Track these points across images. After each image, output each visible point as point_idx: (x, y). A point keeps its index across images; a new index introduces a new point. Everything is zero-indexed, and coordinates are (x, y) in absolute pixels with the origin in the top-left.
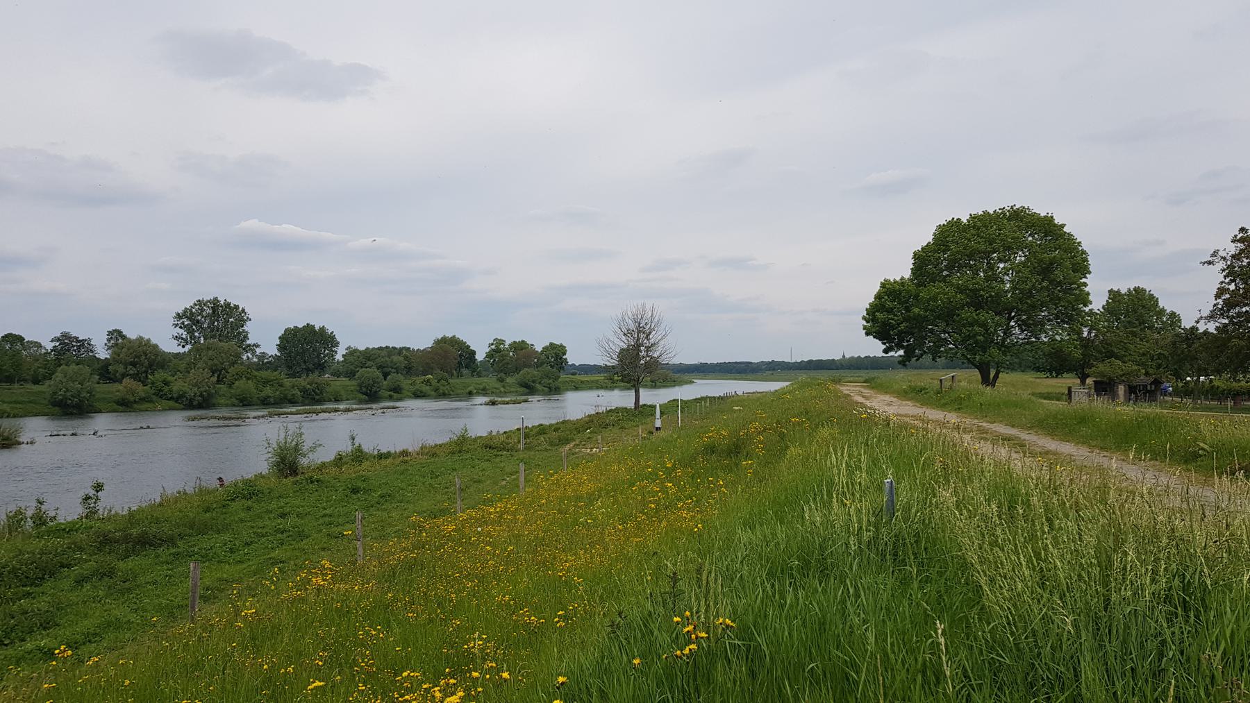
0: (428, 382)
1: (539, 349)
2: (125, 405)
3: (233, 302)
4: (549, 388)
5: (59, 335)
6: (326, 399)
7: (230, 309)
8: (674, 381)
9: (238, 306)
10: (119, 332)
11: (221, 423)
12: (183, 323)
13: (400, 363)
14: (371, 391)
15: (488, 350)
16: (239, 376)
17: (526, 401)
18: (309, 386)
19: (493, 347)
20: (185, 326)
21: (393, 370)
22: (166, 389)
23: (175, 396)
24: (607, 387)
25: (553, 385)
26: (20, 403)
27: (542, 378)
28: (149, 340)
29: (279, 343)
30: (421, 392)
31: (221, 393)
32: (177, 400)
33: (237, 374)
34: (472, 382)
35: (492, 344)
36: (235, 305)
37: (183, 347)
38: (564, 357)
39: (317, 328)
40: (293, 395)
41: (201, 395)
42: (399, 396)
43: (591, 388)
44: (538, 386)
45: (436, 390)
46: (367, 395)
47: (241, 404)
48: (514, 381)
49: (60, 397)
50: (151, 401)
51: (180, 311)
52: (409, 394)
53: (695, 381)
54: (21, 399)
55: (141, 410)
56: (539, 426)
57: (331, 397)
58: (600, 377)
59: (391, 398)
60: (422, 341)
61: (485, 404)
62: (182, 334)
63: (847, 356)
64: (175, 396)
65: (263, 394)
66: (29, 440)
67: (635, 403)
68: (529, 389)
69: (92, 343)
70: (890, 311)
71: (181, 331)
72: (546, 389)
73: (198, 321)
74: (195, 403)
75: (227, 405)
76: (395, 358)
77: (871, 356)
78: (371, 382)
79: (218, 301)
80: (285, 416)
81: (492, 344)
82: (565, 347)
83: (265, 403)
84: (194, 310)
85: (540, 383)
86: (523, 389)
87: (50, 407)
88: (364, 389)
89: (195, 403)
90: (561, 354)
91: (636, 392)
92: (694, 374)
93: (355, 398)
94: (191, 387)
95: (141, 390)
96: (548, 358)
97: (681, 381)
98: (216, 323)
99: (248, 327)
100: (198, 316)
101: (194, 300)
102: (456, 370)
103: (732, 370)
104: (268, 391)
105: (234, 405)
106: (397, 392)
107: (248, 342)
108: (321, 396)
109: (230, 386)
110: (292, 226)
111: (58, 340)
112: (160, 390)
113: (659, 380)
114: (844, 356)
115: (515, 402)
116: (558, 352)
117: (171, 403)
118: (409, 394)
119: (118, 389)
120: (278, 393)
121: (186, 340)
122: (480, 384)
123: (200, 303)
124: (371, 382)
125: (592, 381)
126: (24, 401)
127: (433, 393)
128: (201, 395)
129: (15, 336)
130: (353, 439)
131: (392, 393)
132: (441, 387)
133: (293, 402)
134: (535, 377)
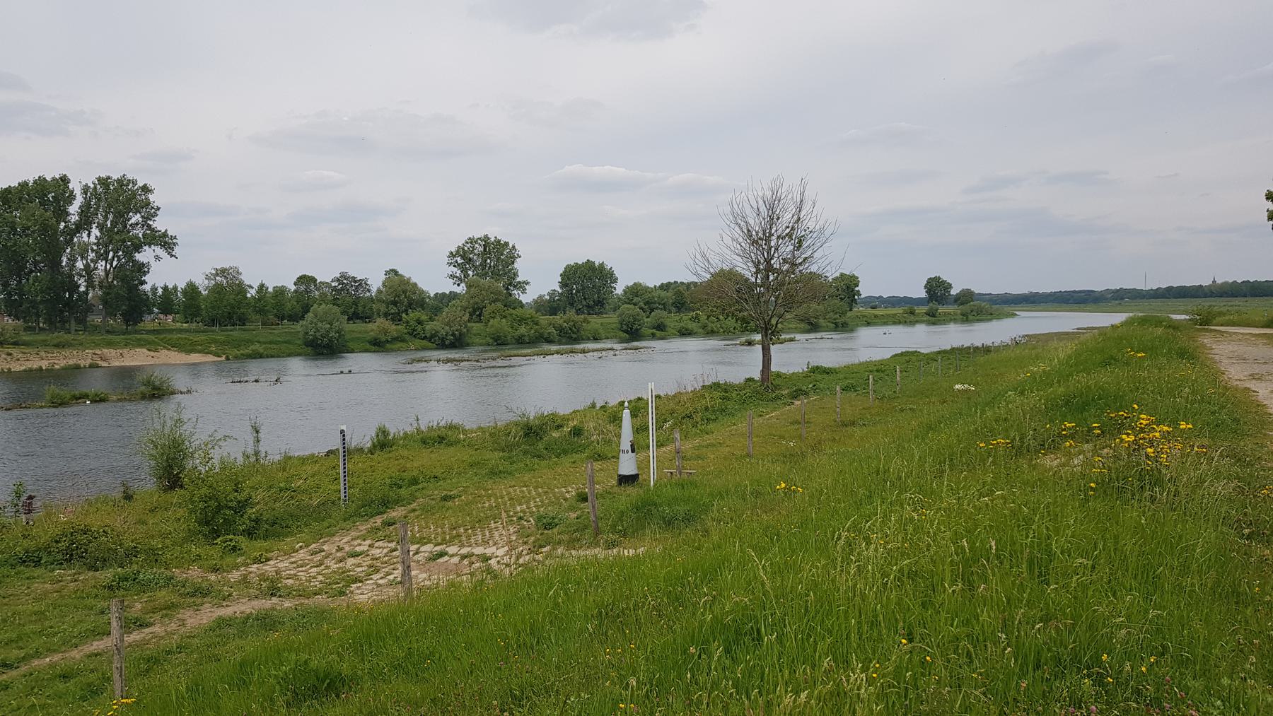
0: (696, 319)
2: (378, 345)
4: (835, 324)
5: (338, 275)
6: (584, 337)
8: (992, 314)
9: (508, 243)
12: (457, 262)
14: (631, 329)
18: (565, 324)
21: (661, 307)
22: (419, 328)
23: (428, 335)
24: (905, 322)
26: (275, 344)
28: (409, 279)
29: (560, 280)
30: (686, 330)
32: (430, 339)
37: (458, 285)
38: (857, 289)
41: (453, 335)
45: (704, 327)
47: (496, 343)
50: (403, 341)
51: (453, 250)
53: (1017, 313)
55: (393, 350)
57: (589, 335)
58: (898, 311)
59: (653, 337)
63: (1219, 281)
64: (428, 335)
66: (185, 390)
67: (763, 371)
69: (368, 283)
71: (455, 270)
73: (470, 260)
74: (447, 342)
75: (481, 345)
78: (631, 319)
79: (489, 239)
80: (508, 358)
83: (521, 342)
84: (466, 248)
87: (304, 346)
88: (625, 327)
89: (447, 342)
91: (763, 349)
92: (1022, 305)
93: (616, 337)
95: (394, 329)
97: (1000, 314)
98: (489, 261)
99: (518, 265)
100: (470, 254)
103: (1069, 300)
104: (523, 330)
105: (489, 345)
106: (660, 331)
107: (518, 279)
110: (608, 167)
111: (338, 280)
112: (414, 330)
113: (972, 314)
114: (1214, 281)
117: (425, 342)
120: (532, 331)
121: (460, 279)
123: (472, 241)
124: (631, 319)
125: (889, 316)
126: (279, 341)
127: (701, 330)
128: (453, 335)
129: (309, 277)
131: (654, 331)
132: (710, 324)
133: (550, 341)
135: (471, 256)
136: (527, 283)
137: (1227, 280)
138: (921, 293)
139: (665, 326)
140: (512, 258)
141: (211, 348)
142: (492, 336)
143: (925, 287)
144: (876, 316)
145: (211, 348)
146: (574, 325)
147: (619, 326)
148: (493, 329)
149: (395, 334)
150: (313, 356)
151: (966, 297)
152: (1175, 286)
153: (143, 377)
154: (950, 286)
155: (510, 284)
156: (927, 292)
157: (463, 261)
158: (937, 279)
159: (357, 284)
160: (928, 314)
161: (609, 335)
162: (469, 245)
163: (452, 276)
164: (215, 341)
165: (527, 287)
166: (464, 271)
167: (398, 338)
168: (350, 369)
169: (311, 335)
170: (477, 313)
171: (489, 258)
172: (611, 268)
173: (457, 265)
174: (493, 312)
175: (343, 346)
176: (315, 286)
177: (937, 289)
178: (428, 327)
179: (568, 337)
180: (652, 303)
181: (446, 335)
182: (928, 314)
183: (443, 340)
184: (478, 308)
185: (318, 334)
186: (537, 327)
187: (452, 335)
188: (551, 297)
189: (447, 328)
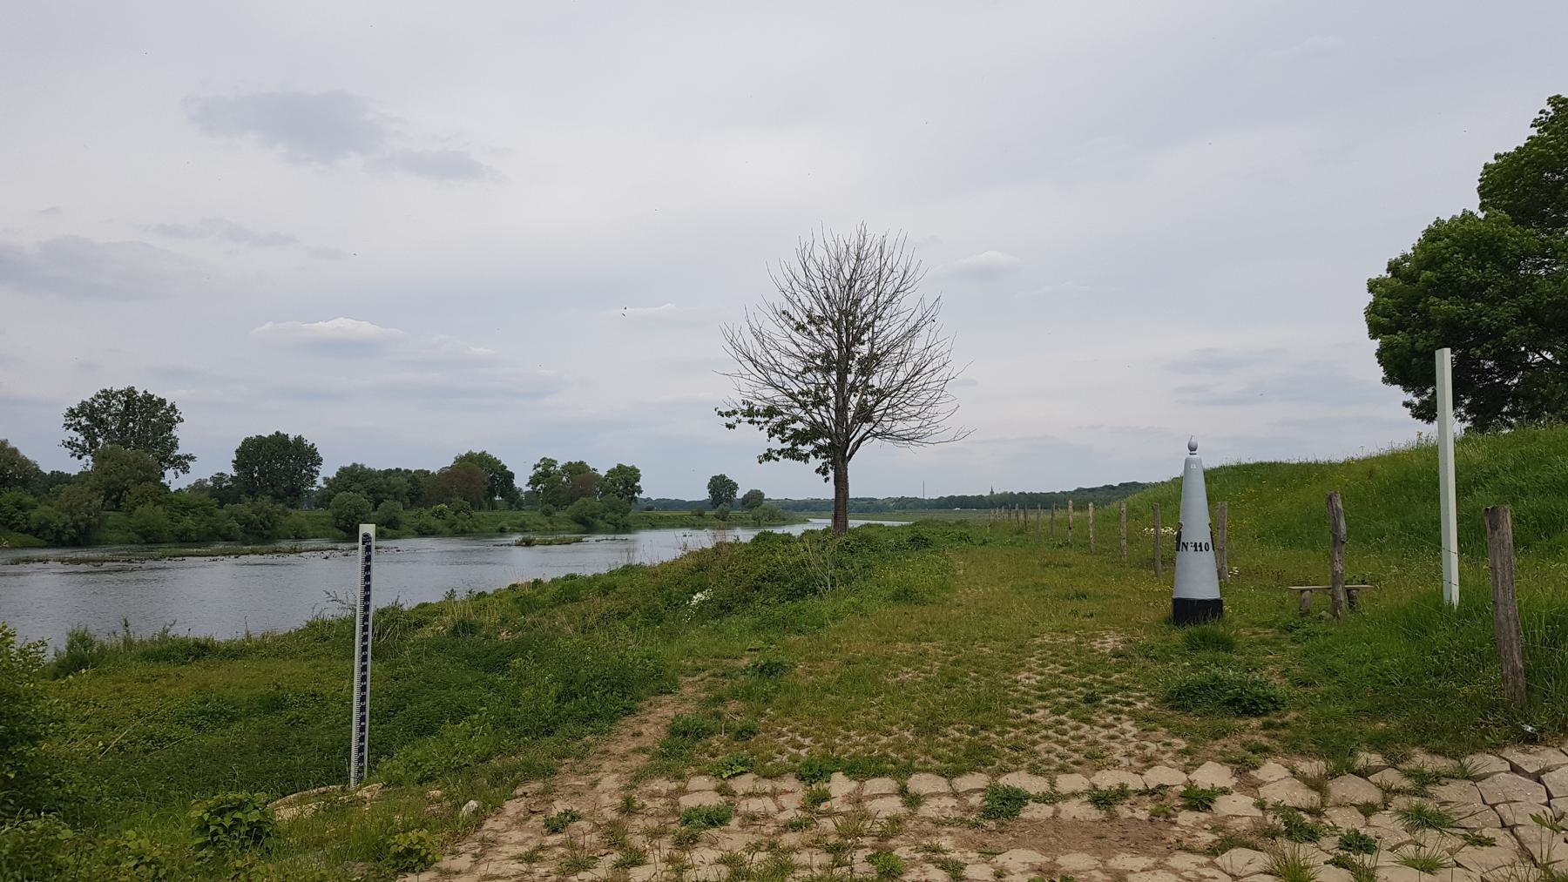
1: (603, 473)
3: (158, 394)
7: (151, 404)
9: (165, 400)
11: (90, 567)
12: (79, 423)
13: (401, 485)
15: (532, 474)
16: (142, 500)
17: (579, 541)
19: (540, 469)
20: (82, 428)
22: (19, 515)
23: (34, 526)
24: (694, 525)
25: (620, 521)
27: (605, 511)
29: (235, 459)
30: (428, 528)
31: (109, 523)
33: (142, 496)
34: (506, 516)
35: (539, 466)
36: (160, 399)
37: (80, 457)
38: (637, 484)
39: (291, 438)
40: (229, 528)
41: (76, 526)
42: (395, 532)
43: (673, 526)
44: (599, 522)
45: (451, 525)
46: (345, 531)
48: (566, 515)
52: (411, 530)
53: (811, 520)
56: (566, 578)
57: (289, 532)
60: (435, 459)
61: (517, 545)
62: (77, 440)
64: (34, 526)
65: (180, 527)
68: (587, 525)
70: (1472, 291)
71: (77, 434)
72: (612, 526)
73: (102, 421)
74: (66, 537)
75: (120, 543)
76: (393, 480)
77: (1027, 492)
78: (353, 512)
79: (135, 393)
80: (180, 558)
81: (539, 466)
82: (638, 471)
84: (96, 405)
85: (602, 518)
86: (577, 527)
88: (342, 523)
89: (66, 537)
90: (632, 479)
94: (60, 513)
96: (615, 485)
98: (131, 425)
99: (178, 432)
100: (103, 413)
101: (98, 390)
102: (485, 499)
104: (188, 522)
105: (132, 543)
107: (177, 453)
108: (273, 530)
109: (130, 513)
112: (11, 518)
114: (992, 492)
115: (561, 543)
116: (629, 477)
117: (28, 538)
118: (411, 530)
122: (518, 519)
123: (107, 395)
124: (353, 512)
125: (675, 518)
127: (447, 529)
128: (76, 526)
133: (227, 538)
134: (595, 509)
135: (104, 416)
136: (192, 458)
138: (704, 495)
143: (709, 487)
144: (661, 518)
146: (267, 517)
148: (142, 519)
151: (755, 498)
152: (687, 500)
154: (735, 486)
155: (164, 459)
156: (710, 492)
161: (318, 533)
163: (70, 444)
165: (190, 464)
166: (91, 437)
170: (114, 497)
171: (132, 421)
172: (313, 444)
174: (142, 496)
177: (721, 487)
178: (34, 514)
179: (257, 534)
180: (377, 492)
183: (59, 533)
184: (114, 491)
186: (211, 519)
187: (74, 527)
189: (67, 516)
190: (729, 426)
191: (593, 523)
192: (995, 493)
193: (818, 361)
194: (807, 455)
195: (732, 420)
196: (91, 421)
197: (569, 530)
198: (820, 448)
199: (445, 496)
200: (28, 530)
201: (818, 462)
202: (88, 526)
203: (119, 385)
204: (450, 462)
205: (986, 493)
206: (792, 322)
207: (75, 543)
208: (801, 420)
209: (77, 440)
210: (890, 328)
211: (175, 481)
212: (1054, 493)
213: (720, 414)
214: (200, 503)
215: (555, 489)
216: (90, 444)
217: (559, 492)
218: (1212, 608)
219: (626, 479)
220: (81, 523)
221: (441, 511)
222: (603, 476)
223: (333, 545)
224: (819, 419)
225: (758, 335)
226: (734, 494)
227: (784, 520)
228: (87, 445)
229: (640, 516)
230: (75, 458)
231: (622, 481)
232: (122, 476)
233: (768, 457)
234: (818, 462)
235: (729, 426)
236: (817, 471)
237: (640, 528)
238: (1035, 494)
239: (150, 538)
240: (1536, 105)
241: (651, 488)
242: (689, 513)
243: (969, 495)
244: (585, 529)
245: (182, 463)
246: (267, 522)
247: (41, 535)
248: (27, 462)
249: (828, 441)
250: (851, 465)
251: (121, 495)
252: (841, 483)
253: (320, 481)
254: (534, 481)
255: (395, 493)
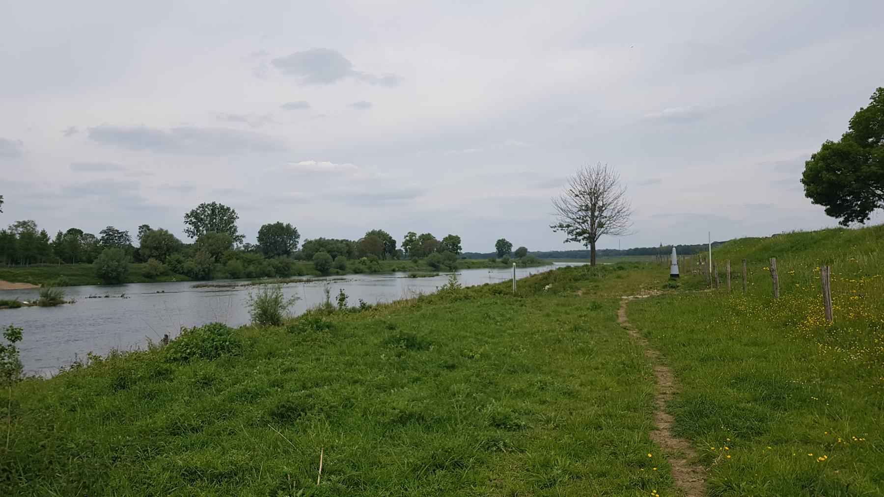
4: (450, 267)
5: (105, 228)
7: (224, 210)
9: (229, 208)
10: (147, 226)
11: (217, 289)
12: (191, 220)
14: (324, 268)
15: (404, 240)
18: (280, 265)
19: (408, 238)
20: (193, 223)
21: (340, 254)
22: (179, 266)
23: (186, 271)
25: (452, 265)
27: (444, 260)
30: (359, 269)
34: (395, 263)
35: (407, 236)
37: (192, 237)
38: (459, 245)
39: (285, 225)
41: (204, 271)
42: (344, 272)
43: (479, 268)
45: (370, 268)
49: (104, 271)
51: (189, 213)
52: (351, 271)
53: (554, 263)
54: (77, 273)
55: (160, 281)
57: (296, 273)
60: (356, 235)
68: (435, 268)
69: (128, 234)
71: (191, 226)
73: (202, 219)
74: (200, 276)
76: (340, 245)
79: (216, 205)
81: (407, 236)
82: (459, 238)
85: (443, 264)
86: (430, 268)
88: (319, 267)
89: (200, 276)
95: (161, 267)
98: (214, 221)
99: (237, 223)
101: (199, 204)
104: (251, 268)
107: (237, 234)
109: (225, 264)
114: (661, 245)
117: (183, 276)
119: (144, 267)
120: (258, 269)
121: (193, 233)
123: (203, 206)
125: (480, 263)
127: (367, 270)
128: (204, 271)
130: (328, 293)
136: (244, 237)
137: (669, 244)
138: (493, 249)
139: (345, 267)
140: (232, 219)
141: (29, 279)
142: (230, 272)
143: (496, 246)
144: (473, 263)
145: (29, 279)
147: (315, 266)
149: (162, 270)
150: (246, 278)
151: (522, 252)
152: (482, 253)
153: (486, 289)
154: (511, 245)
156: (497, 249)
157: (195, 220)
158: (503, 240)
159: (119, 235)
160: (503, 262)
162: (201, 209)
163: (188, 231)
164: (31, 274)
165: (243, 239)
166: (197, 227)
167: (164, 273)
168: (163, 290)
169: (104, 270)
172: (295, 228)
173: (191, 223)
175: (125, 278)
176: (82, 236)
177: (503, 246)
180: (332, 252)
181: (199, 271)
182: (503, 262)
183: (197, 275)
185: (109, 269)
187: (203, 271)
188: (245, 249)
190: (554, 231)
191: (438, 266)
192: (663, 246)
193: (584, 208)
194: (580, 240)
195: (555, 229)
196: (196, 219)
197: (427, 270)
198: (585, 238)
199: (362, 253)
200: (183, 273)
201: (585, 242)
202: (209, 270)
203: (209, 201)
204: (363, 236)
205: (658, 246)
206: (573, 194)
207: (203, 279)
208: (579, 229)
209: (191, 229)
210: (609, 197)
211: (50, 241)
212: (699, 245)
213: (552, 227)
214: (256, 259)
215: (416, 249)
216: (197, 231)
217: (418, 250)
218: (677, 275)
219: (453, 242)
220: (206, 269)
221: (364, 261)
222: (441, 241)
223: (316, 279)
224: (585, 228)
225: (565, 201)
226: (510, 249)
227: (539, 263)
228: (195, 231)
229: (461, 262)
230: (190, 237)
231: (451, 244)
232: (218, 246)
233: (567, 241)
234: (585, 242)
235: (554, 231)
236: (584, 245)
237: (462, 268)
238: (688, 246)
239: (236, 276)
240: (872, 91)
241: (466, 247)
242: (487, 260)
243: (647, 247)
244: (434, 269)
245: (239, 239)
246: (286, 268)
247: (189, 275)
248: (177, 240)
249: (588, 235)
250: (596, 243)
251: (218, 256)
252: (593, 247)
253: (300, 246)
254: (405, 244)
255: (341, 252)
